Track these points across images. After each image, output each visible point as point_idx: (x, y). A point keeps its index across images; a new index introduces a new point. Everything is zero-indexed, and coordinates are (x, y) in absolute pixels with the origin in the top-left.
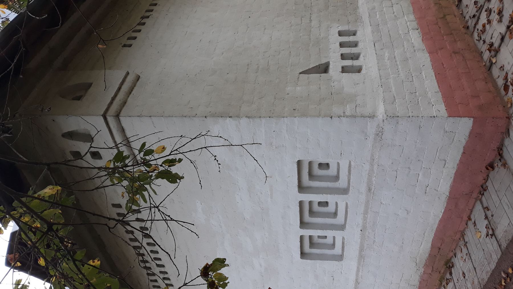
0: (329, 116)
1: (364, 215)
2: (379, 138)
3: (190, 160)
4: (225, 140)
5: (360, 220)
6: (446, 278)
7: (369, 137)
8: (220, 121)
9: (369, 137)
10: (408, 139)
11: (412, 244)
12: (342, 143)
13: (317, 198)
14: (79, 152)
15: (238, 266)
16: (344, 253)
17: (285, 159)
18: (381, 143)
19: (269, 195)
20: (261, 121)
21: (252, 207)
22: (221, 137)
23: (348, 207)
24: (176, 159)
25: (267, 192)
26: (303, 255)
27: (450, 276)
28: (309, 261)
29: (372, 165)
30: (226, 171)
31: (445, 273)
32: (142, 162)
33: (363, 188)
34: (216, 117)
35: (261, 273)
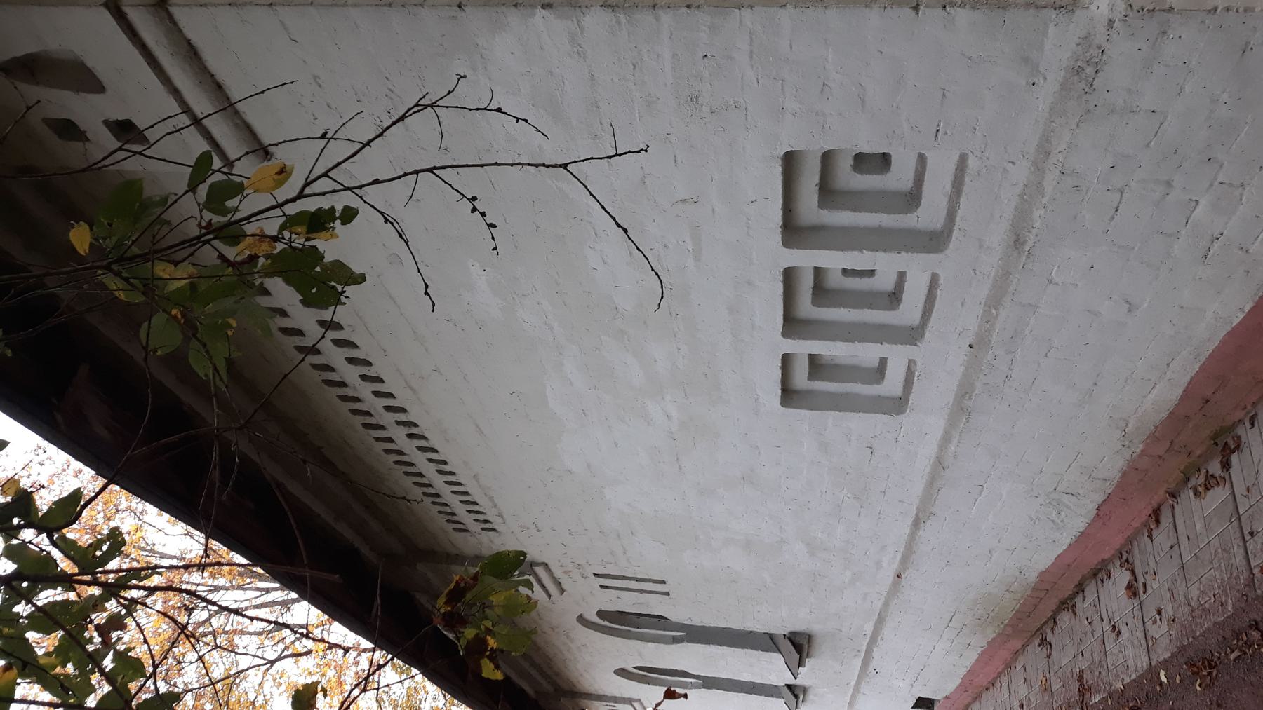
0: (907, 4)
1: (987, 308)
2: (1083, 85)
3: (381, 213)
4: (518, 119)
5: (971, 321)
6: (1207, 471)
7: (1045, 79)
8: (509, 20)
9: (1045, 79)
10: (1187, 89)
11: (1124, 387)
12: (944, 95)
13: (833, 260)
14: (69, 120)
15: (606, 417)
16: (911, 398)
17: (744, 148)
18: (1087, 101)
19: (691, 249)
20: (657, 19)
21: (637, 282)
22: (499, 110)
23: (937, 283)
24: (333, 209)
25: (683, 243)
26: (789, 395)
27: (1222, 471)
28: (804, 412)
29: (1038, 169)
30: (550, 182)
31: (1205, 458)
32: (204, 228)
33: (998, 235)
34: (497, 6)
35: (672, 433)
